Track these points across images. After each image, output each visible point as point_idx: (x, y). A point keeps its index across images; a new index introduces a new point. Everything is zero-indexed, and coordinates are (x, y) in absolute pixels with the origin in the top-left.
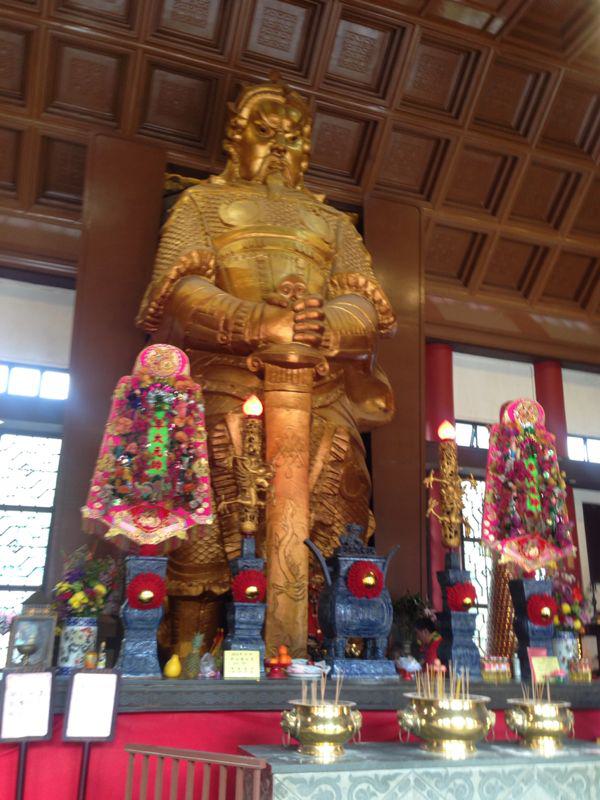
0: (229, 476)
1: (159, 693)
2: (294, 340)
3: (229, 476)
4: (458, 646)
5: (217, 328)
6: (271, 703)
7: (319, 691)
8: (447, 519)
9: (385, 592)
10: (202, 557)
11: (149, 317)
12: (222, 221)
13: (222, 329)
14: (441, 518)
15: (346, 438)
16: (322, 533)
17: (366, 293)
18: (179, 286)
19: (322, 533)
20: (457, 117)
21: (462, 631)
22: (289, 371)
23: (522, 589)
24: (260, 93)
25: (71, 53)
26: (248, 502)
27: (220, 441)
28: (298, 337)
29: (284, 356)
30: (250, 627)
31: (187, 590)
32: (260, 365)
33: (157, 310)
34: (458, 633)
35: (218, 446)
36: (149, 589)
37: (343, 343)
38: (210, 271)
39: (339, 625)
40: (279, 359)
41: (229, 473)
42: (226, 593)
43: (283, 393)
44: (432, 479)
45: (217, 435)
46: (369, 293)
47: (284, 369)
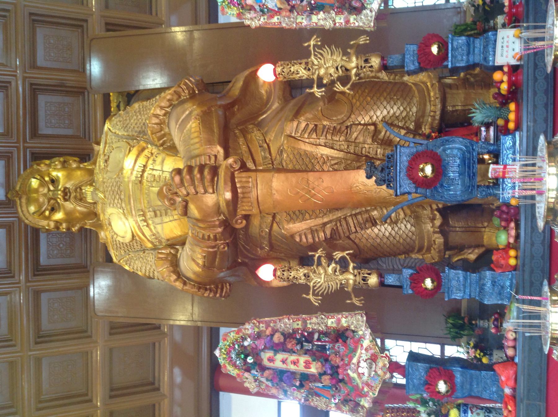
0: (338, 224)
1: (529, 391)
2: (214, 192)
3: (338, 224)
4: (485, 59)
5: (215, 252)
6: (543, 243)
7: (531, 303)
8: (354, 71)
9: (423, 393)
10: (409, 226)
11: (218, 295)
12: (131, 241)
13: (216, 249)
14: (354, 78)
15: (295, 124)
16: (383, 133)
17: (165, 115)
18: (188, 279)
19: (383, 133)
20: (8, 11)
21: (468, 54)
22: (240, 195)
23: (396, 363)
24: (24, 215)
25: (45, 325)
26: (351, 282)
27: (310, 236)
28: (211, 191)
29: (227, 202)
30: (468, 284)
31: (439, 247)
32: (241, 218)
33: (211, 290)
34: (471, 58)
35: (313, 238)
36: (437, 385)
37: (210, 142)
38: (172, 251)
39: (467, 64)
40: (231, 208)
41: (336, 225)
42: (441, 214)
43: (259, 199)
44: (315, 89)
45: (304, 240)
46: (163, 112)
47: (239, 199)
